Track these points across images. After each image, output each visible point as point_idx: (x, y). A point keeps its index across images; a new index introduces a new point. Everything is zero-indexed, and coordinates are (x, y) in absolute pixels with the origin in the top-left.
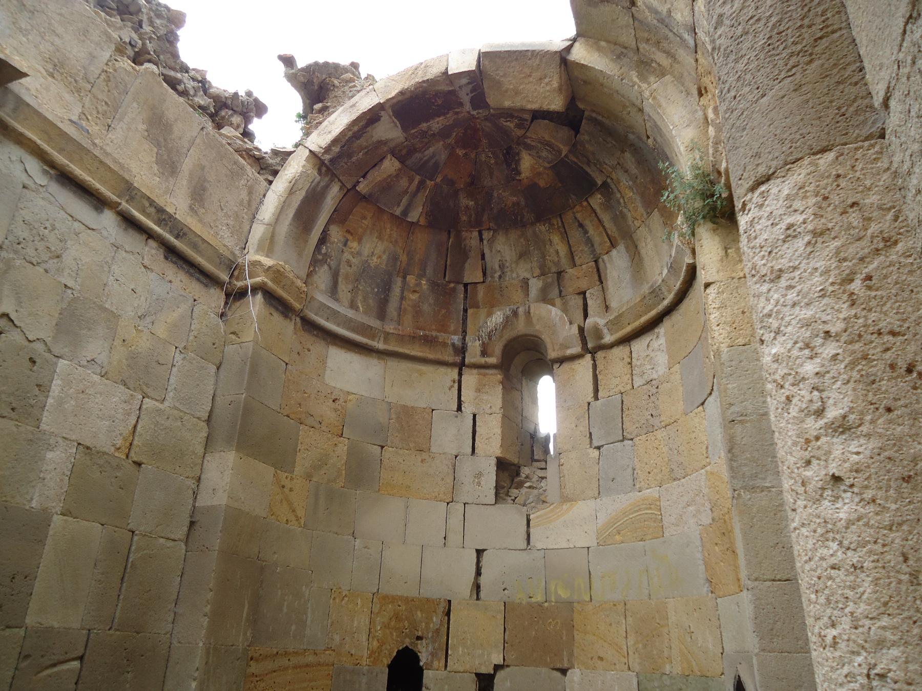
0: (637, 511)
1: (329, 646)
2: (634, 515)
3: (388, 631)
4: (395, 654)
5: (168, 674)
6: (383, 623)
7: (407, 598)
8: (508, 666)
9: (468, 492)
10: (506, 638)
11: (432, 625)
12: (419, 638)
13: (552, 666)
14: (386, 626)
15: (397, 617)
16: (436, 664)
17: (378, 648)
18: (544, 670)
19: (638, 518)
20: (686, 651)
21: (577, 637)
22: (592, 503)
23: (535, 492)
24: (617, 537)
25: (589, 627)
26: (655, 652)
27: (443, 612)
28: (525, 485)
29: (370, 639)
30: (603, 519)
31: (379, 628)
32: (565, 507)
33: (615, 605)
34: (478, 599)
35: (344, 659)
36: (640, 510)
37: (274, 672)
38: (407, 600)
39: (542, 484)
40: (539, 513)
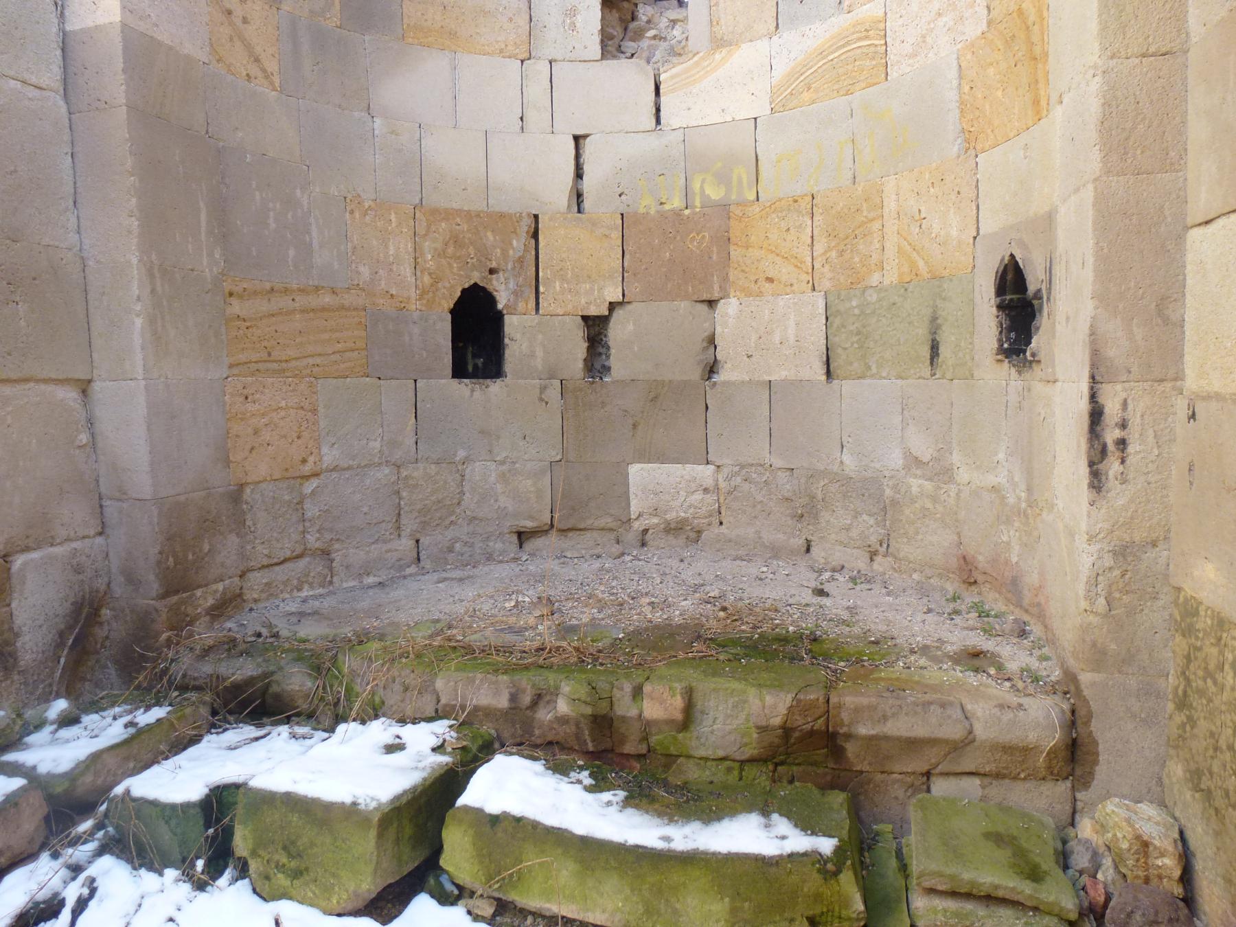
0: (843, 46)
1: (356, 283)
2: (836, 54)
3: (444, 261)
4: (459, 294)
5: (91, 310)
6: (436, 249)
7: (469, 212)
8: (629, 303)
9: (553, 42)
10: (626, 264)
11: (511, 252)
12: (492, 271)
13: (695, 298)
14: (440, 254)
15: (456, 240)
16: (521, 306)
17: (432, 285)
18: (684, 305)
19: (843, 57)
20: (908, 247)
21: (735, 253)
22: (763, 46)
23: (663, 45)
24: (805, 94)
25: (753, 238)
26: (857, 259)
27: (527, 232)
28: (647, 35)
29: (418, 273)
30: (780, 71)
31: (429, 257)
32: (718, 56)
33: (796, 201)
34: (579, 211)
35: (382, 301)
36: (848, 43)
37: (273, 315)
38: (469, 216)
39: (675, 32)
40: (674, 71)
